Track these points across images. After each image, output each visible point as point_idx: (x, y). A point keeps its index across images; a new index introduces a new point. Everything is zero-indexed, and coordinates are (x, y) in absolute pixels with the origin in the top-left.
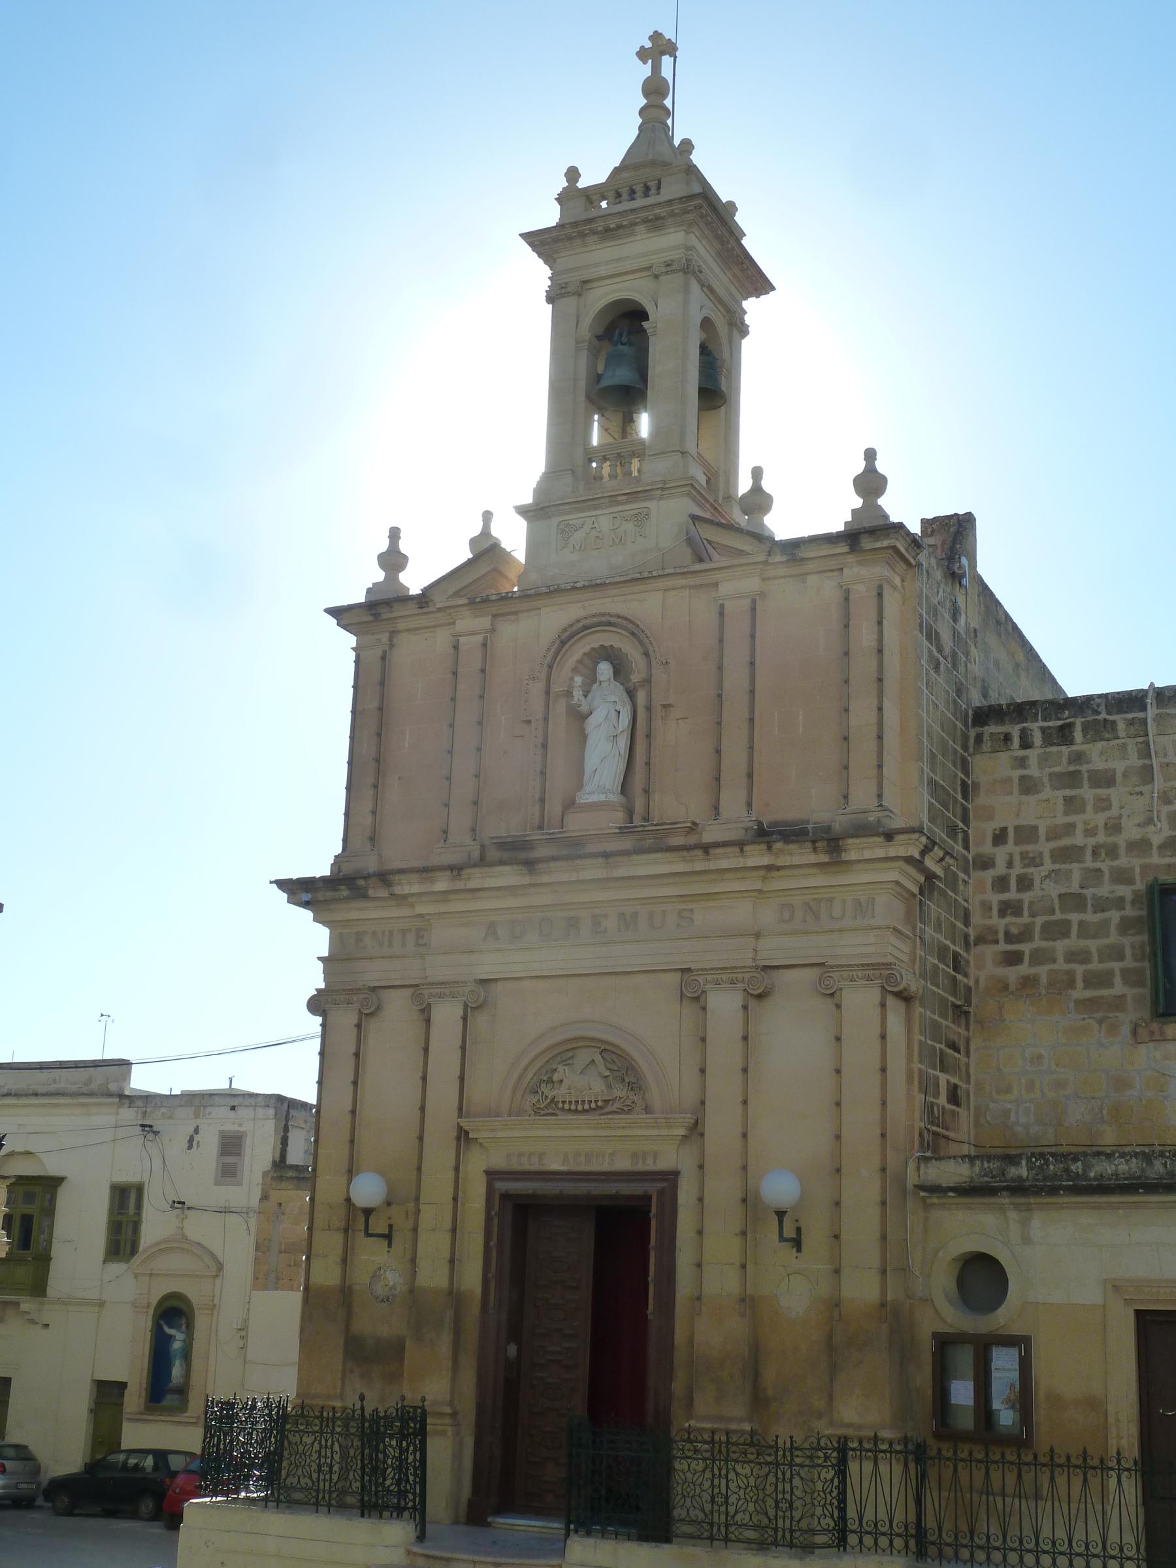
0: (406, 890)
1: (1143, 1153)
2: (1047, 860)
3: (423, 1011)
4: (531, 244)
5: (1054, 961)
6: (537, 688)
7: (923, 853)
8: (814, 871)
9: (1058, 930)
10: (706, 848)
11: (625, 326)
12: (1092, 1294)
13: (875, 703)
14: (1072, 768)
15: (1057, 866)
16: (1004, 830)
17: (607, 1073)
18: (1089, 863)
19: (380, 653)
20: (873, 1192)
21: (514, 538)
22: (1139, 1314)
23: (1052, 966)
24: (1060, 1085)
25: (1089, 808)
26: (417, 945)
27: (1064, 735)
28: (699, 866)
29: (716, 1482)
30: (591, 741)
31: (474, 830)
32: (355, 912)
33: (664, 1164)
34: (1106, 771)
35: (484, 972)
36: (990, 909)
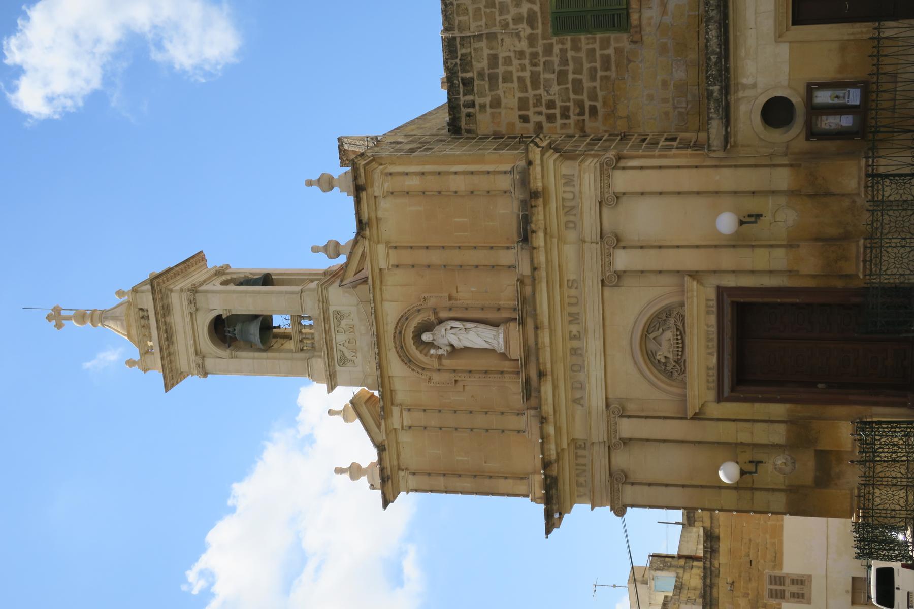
0: (553, 452)
1: (706, 22)
2: (538, 92)
3: (624, 443)
4: (173, 385)
5: (595, 88)
6: (436, 377)
7: (538, 147)
8: (547, 209)
9: (578, 84)
10: (534, 269)
11: (224, 330)
12: (784, 49)
13: (452, 176)
14: (487, 79)
15: (542, 86)
16: (520, 117)
17: (661, 330)
18: (540, 68)
19: (411, 477)
20: (726, 172)
21: (344, 394)
22: (793, 24)
23: (598, 89)
24: (665, 84)
25: (510, 68)
26: (585, 448)
27: (468, 83)
28: (544, 274)
29: (893, 245)
30: (468, 344)
31: (518, 414)
32: (565, 485)
33: (713, 295)
34: (489, 59)
35: (601, 404)
36: (565, 124)
